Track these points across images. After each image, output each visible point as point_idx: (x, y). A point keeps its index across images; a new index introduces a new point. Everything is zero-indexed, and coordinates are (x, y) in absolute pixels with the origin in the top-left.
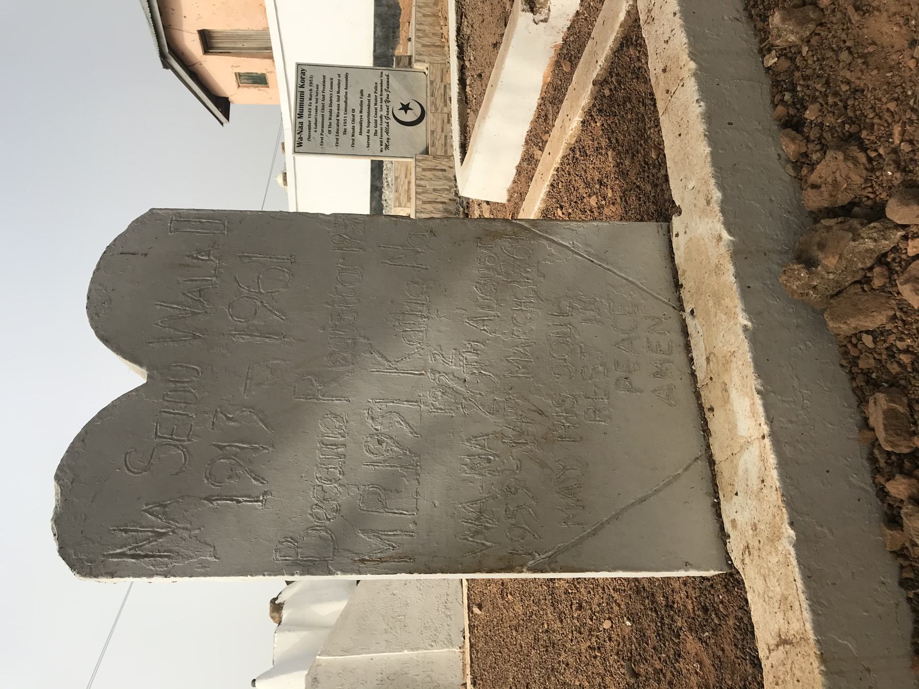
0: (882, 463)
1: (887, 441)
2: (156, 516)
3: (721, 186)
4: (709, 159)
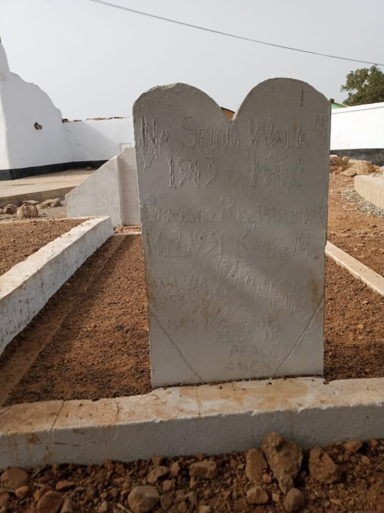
0: (188, 462)
1: (193, 467)
2: (162, 137)
3: (329, 410)
4: (346, 405)
